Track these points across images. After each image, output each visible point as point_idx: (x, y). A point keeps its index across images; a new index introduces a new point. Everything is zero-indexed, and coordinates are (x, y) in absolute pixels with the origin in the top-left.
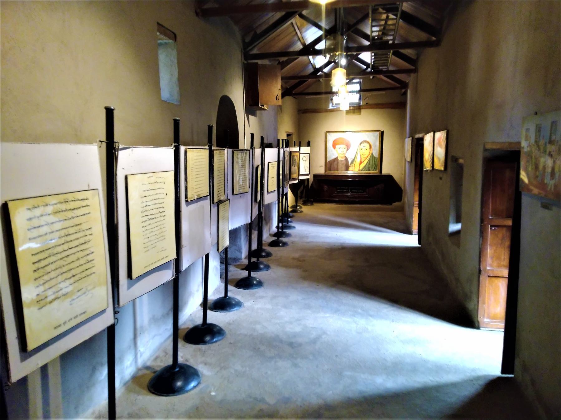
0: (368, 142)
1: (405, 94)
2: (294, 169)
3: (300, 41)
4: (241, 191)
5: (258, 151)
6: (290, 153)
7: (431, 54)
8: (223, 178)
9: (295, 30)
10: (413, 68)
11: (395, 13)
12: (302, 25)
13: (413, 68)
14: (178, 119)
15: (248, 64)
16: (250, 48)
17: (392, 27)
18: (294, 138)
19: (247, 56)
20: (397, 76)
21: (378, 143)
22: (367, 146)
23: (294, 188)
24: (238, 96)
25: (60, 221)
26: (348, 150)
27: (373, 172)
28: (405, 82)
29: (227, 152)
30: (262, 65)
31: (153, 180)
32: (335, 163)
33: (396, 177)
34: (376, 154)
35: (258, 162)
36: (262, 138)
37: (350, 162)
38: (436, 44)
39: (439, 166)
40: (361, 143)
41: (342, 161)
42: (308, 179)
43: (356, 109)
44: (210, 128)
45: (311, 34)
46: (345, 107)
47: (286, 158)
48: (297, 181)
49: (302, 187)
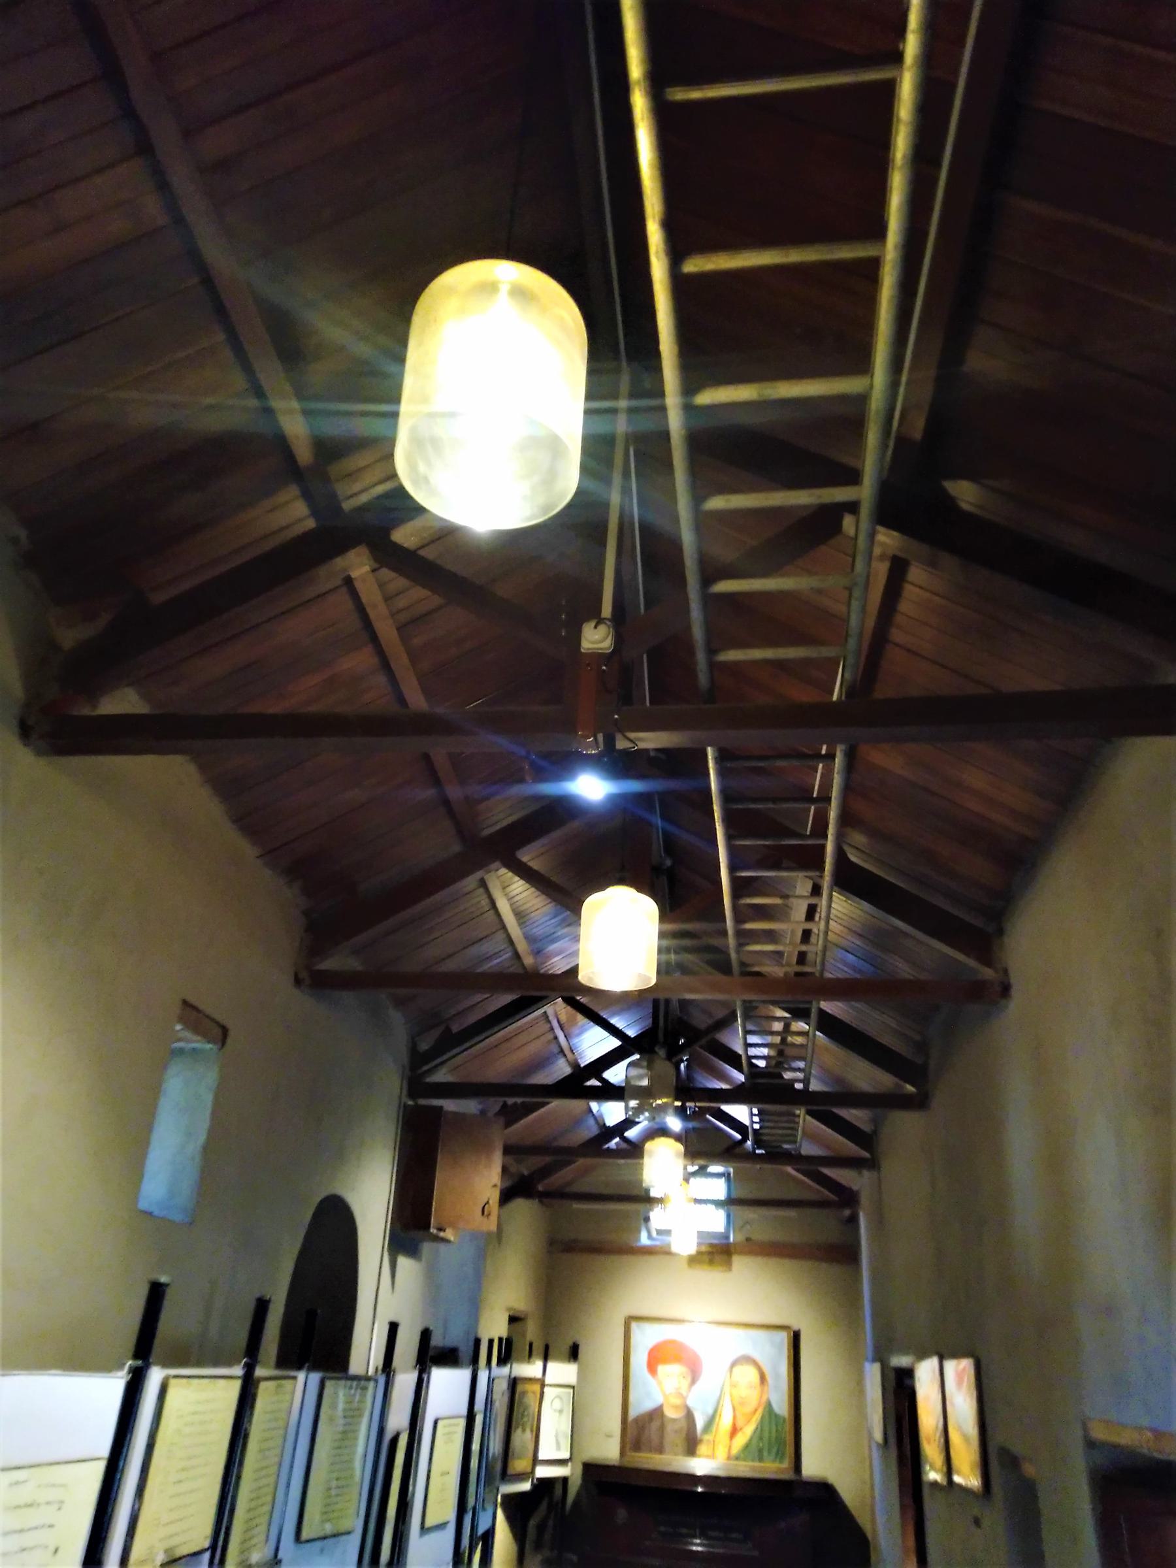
0: (755, 1363)
1: (853, 1220)
2: (522, 1438)
3: (565, 1055)
4: (328, 1528)
5: (405, 1381)
6: (514, 1383)
7: (905, 1126)
8: (272, 1480)
9: (552, 1029)
10: (867, 1155)
11: (754, 1070)
12: (573, 1022)
13: (867, 1155)
14: (163, 1279)
15: (417, 1107)
16: (425, 1068)
17: (799, 1040)
18: (532, 1331)
19: (416, 1085)
20: (826, 1171)
21: (784, 1368)
22: (751, 1374)
23: (517, 1508)
24: (372, 1198)
25: (356, 494)
26: (693, 1381)
27: (773, 1468)
28: (850, 1190)
29: (304, 1381)
30: (455, 1114)
31: (25, 1494)
32: (655, 1425)
33: (848, 1492)
34: (782, 1406)
35: (398, 1419)
36: (426, 1335)
37: (700, 1424)
38: (919, 1102)
39: (968, 1477)
40: (731, 1371)
41: (674, 1420)
42: (565, 1480)
43: (717, 1253)
44: (262, 1307)
45: (594, 1043)
46: (685, 1244)
47: (497, 1404)
48: (526, 1486)
49: (544, 1506)
